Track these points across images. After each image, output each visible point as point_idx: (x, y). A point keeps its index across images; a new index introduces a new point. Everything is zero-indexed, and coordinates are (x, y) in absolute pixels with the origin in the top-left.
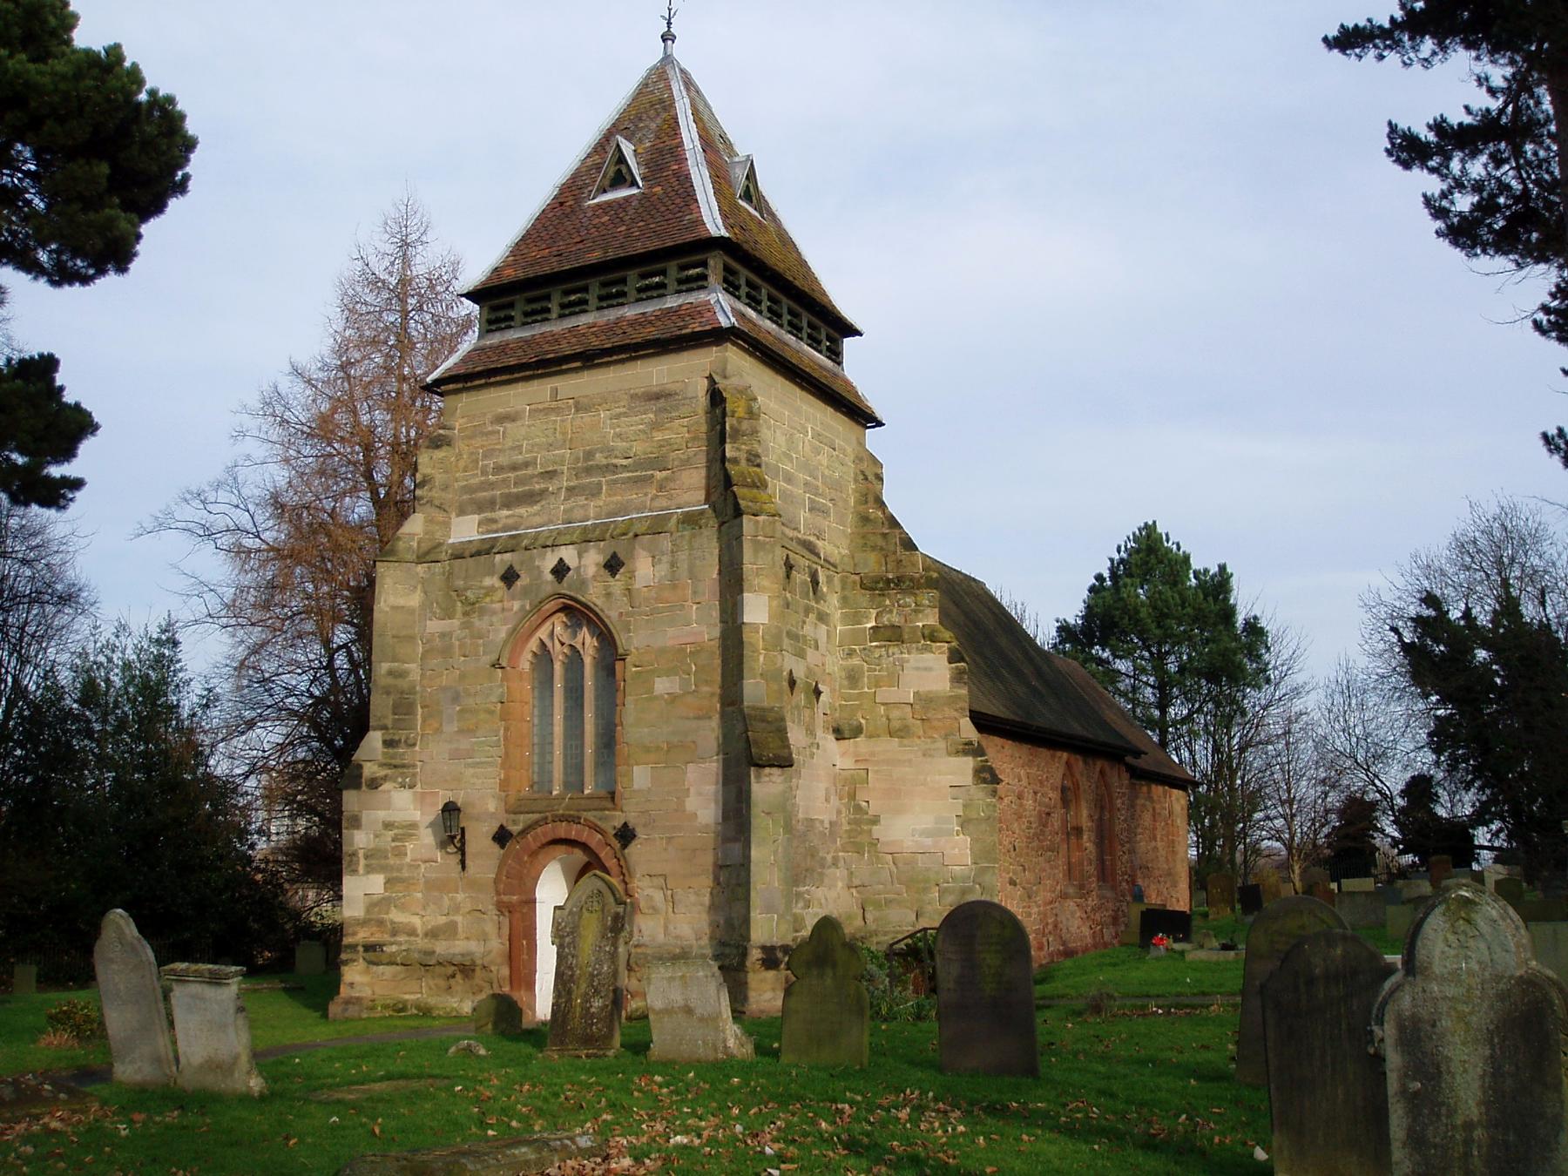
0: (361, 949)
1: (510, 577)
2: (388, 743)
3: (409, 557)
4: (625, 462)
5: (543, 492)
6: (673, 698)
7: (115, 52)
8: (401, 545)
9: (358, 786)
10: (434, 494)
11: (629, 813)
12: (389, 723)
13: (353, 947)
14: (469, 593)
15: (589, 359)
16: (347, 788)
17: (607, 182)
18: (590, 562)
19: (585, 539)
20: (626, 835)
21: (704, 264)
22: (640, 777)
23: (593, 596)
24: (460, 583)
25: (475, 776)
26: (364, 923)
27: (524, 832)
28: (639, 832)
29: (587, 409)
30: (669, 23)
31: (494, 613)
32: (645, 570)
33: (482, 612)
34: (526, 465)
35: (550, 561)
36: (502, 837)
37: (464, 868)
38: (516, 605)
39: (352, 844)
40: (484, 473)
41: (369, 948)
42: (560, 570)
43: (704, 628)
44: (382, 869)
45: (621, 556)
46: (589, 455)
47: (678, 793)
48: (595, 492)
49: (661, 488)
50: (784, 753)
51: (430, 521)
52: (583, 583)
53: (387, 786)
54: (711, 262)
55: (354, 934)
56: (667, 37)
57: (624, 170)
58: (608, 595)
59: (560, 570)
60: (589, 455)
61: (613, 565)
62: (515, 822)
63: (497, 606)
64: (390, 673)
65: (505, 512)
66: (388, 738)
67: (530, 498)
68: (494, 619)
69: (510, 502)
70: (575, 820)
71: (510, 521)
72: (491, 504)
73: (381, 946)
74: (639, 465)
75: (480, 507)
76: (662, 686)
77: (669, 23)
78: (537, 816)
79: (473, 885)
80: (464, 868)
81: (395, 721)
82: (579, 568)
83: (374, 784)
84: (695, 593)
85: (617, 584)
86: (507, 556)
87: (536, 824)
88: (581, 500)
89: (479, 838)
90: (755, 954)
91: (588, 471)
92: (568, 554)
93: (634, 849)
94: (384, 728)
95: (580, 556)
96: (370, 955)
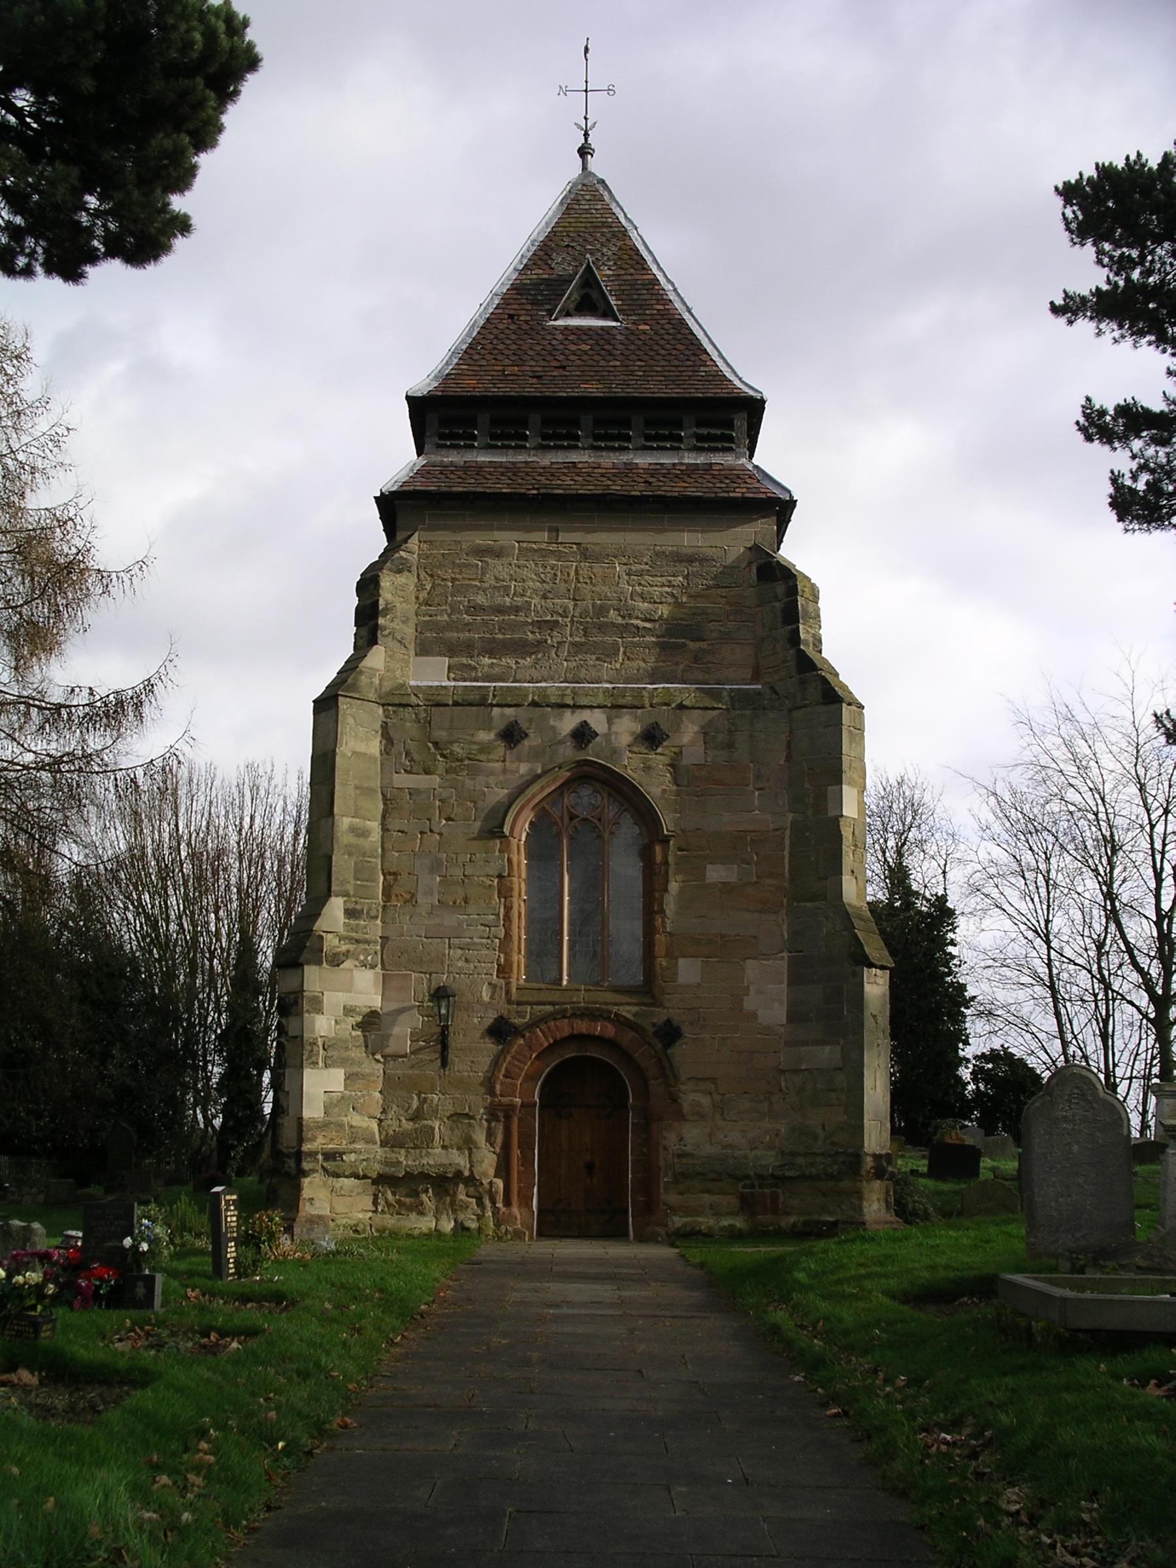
0: (320, 1157)
2: (350, 913)
3: (372, 696)
4: (648, 625)
5: (540, 645)
6: (727, 888)
8: (364, 680)
9: (319, 963)
10: (394, 625)
11: (672, 1009)
12: (350, 888)
13: (313, 1154)
14: (456, 748)
16: (308, 963)
17: (572, 306)
18: (626, 728)
19: (615, 707)
21: (730, 426)
23: (630, 766)
24: (441, 734)
26: (324, 1126)
27: (531, 1026)
28: (685, 1029)
29: (598, 559)
30: (586, 135)
31: (492, 773)
33: (473, 772)
34: (517, 610)
35: (568, 722)
36: (500, 1031)
37: (444, 1063)
39: (313, 1031)
40: (454, 610)
41: (330, 1156)
42: (583, 735)
43: (769, 817)
44: (342, 1062)
45: (665, 727)
49: (696, 659)
51: (391, 656)
52: (614, 753)
53: (348, 964)
54: (737, 423)
55: (314, 1139)
57: (595, 295)
58: (647, 768)
59: (583, 735)
60: (602, 610)
62: (521, 1015)
63: (498, 765)
64: (353, 830)
65: (486, 661)
66: (351, 906)
67: (522, 648)
68: (492, 780)
71: (496, 670)
72: (468, 648)
73: (341, 1154)
75: (450, 650)
77: (586, 135)
78: (549, 1008)
80: (444, 1063)
81: (357, 887)
82: (607, 736)
83: (336, 961)
84: (758, 777)
86: (509, 711)
87: (544, 1019)
88: (591, 660)
89: (469, 1028)
90: (869, 1162)
91: (602, 628)
92: (597, 720)
93: (679, 1051)
94: (346, 894)
95: (610, 721)
96: (329, 1165)
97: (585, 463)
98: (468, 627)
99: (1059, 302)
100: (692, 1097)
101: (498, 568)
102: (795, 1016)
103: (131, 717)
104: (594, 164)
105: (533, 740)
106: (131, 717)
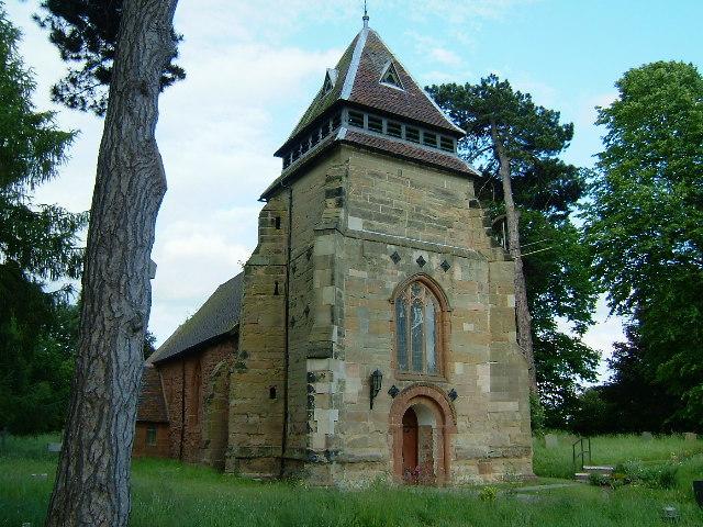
1: (396, 258)
7: (619, 84)
11: (453, 385)
14: (374, 260)
15: (422, 164)
18: (435, 262)
19: (433, 250)
20: (453, 395)
22: (458, 368)
25: (379, 358)
31: (388, 274)
32: (458, 272)
35: (416, 255)
38: (399, 273)
42: (421, 262)
46: (418, 209)
47: (73, 447)
48: (421, 228)
50: (143, 431)
56: (366, 18)
58: (443, 279)
60: (418, 209)
61: (445, 267)
62: (400, 385)
67: (389, 219)
69: (380, 218)
70: (432, 386)
74: (439, 222)
75: (363, 216)
76: (467, 327)
79: (376, 417)
85: (447, 275)
87: (409, 388)
91: (419, 216)
92: (425, 256)
93: (456, 402)
97: (401, 143)
98: (370, 207)
99: (431, 87)
100: (461, 423)
101: (384, 184)
102: (494, 389)
103: (50, 124)
104: (370, 24)
105: (402, 262)
106: (50, 124)
